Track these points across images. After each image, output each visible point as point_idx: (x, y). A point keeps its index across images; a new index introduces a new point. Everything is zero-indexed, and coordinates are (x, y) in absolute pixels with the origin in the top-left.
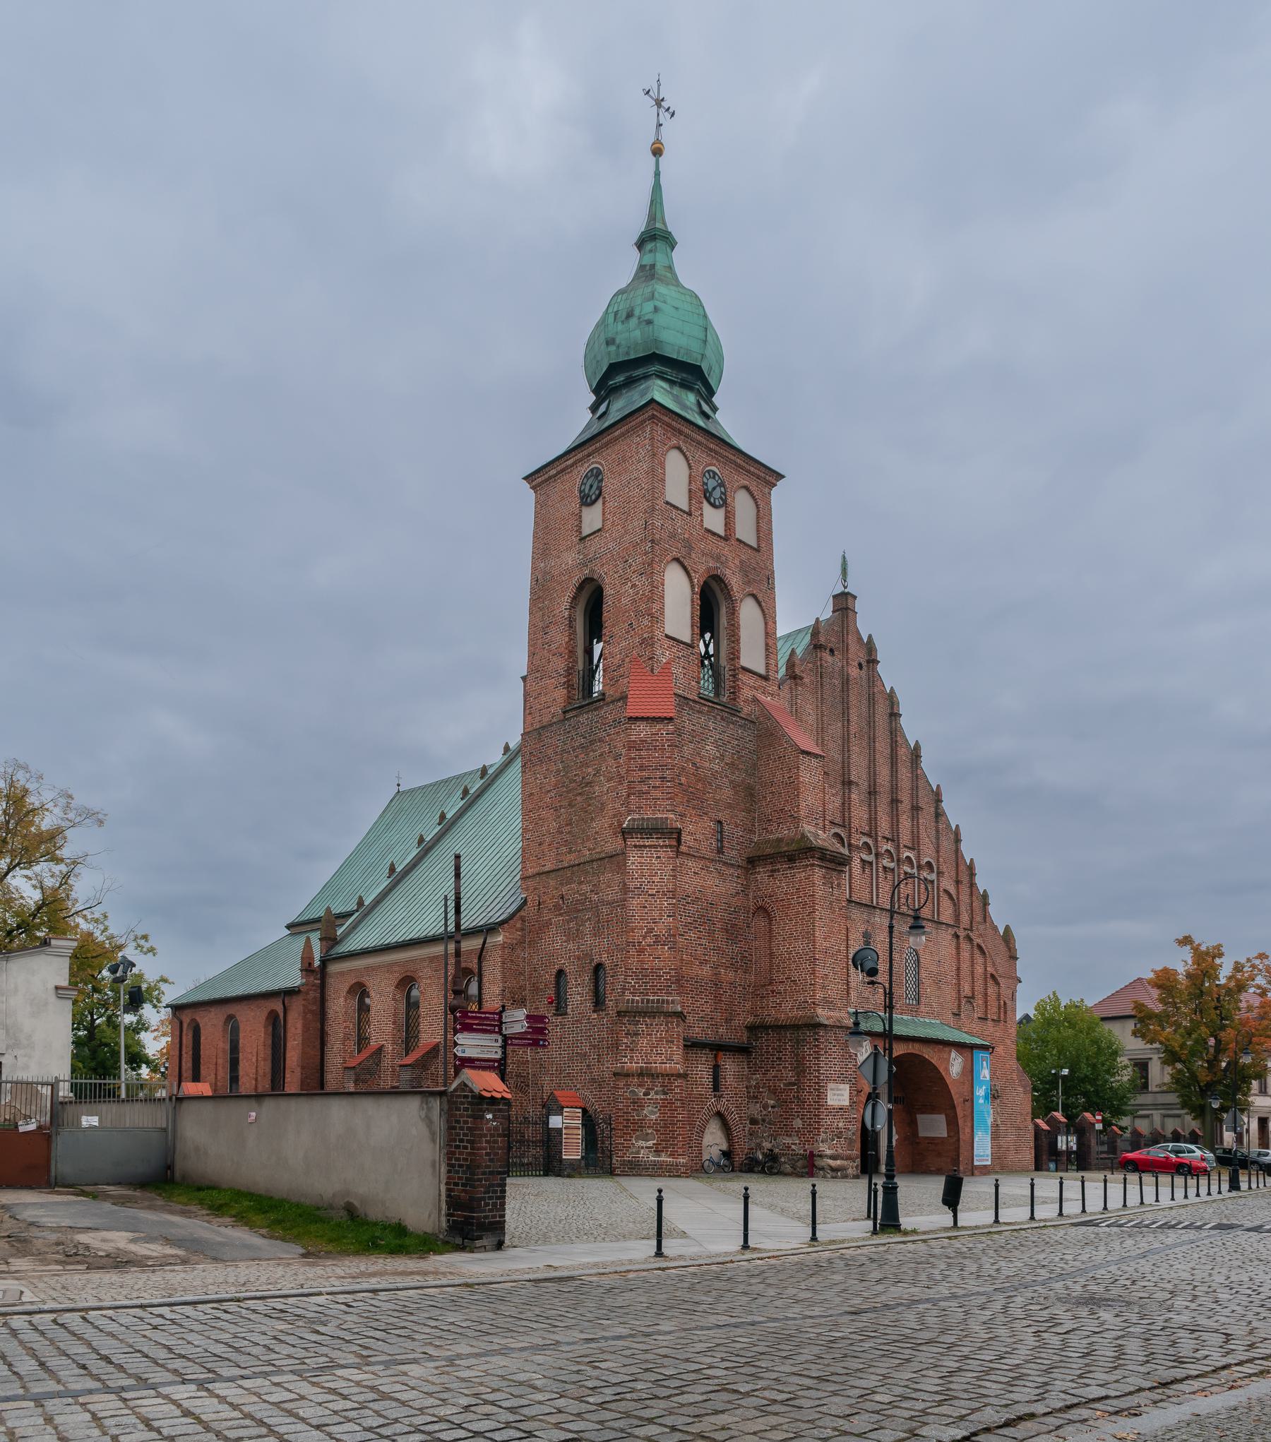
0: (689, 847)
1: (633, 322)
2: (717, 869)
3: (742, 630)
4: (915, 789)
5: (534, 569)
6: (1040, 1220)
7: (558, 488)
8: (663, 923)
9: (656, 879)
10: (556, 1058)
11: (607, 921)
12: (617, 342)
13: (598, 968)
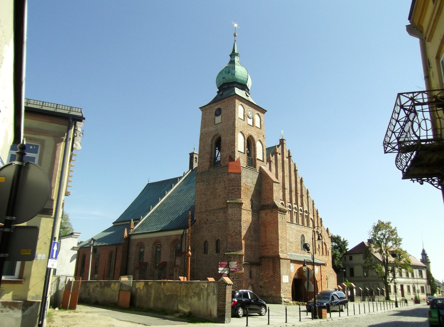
1: (230, 74)
3: (257, 149)
4: (302, 190)
5: (201, 130)
6: (342, 317)
12: (226, 78)
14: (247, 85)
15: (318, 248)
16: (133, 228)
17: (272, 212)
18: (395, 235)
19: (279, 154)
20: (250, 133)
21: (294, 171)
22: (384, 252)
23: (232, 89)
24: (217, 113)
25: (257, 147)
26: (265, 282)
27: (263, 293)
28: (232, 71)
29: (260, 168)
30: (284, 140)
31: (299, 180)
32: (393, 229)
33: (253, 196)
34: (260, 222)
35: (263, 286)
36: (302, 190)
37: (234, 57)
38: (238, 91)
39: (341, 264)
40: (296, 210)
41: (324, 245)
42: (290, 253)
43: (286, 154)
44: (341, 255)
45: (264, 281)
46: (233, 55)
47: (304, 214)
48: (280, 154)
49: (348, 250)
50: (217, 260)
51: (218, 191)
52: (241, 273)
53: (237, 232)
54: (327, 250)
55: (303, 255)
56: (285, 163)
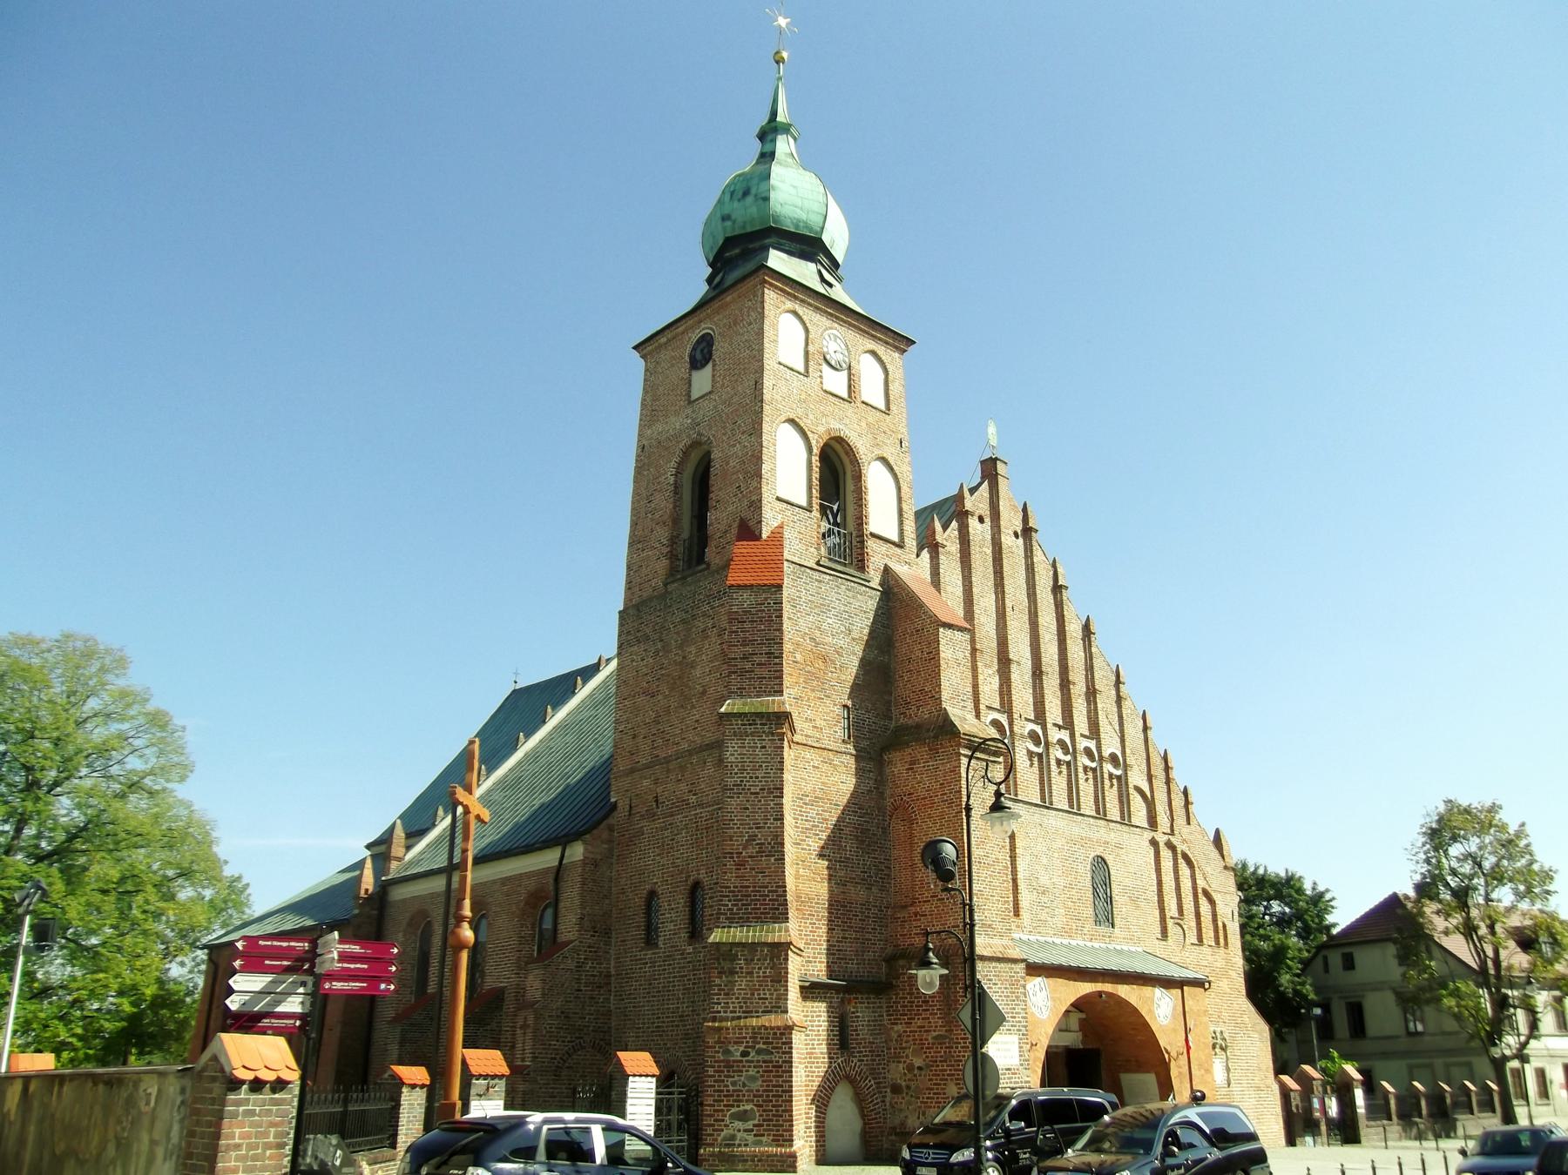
0: (806, 736)
1: (750, 199)
2: (842, 762)
4: (1090, 668)
7: (665, 355)
8: (769, 828)
9: (760, 774)
10: (643, 1006)
11: (706, 828)
12: (733, 217)
13: (696, 886)
14: (824, 238)
15: (1177, 916)
16: (400, 854)
17: (934, 751)
18: (1523, 857)
19: (976, 518)
20: (835, 425)
21: (1049, 589)
22: (1483, 931)
23: (758, 258)
24: (699, 356)
25: (868, 487)
26: (910, 1068)
27: (906, 1117)
28: (758, 189)
29: (887, 570)
30: (998, 462)
31: (1074, 629)
32: (1512, 832)
33: (856, 690)
34: (889, 802)
35: (904, 1084)
36: (1090, 668)
37: (774, 141)
38: (778, 260)
39: (1308, 987)
40: (1066, 752)
41: (1203, 901)
42: (1039, 938)
43: (1011, 521)
44: (1308, 951)
45: (908, 1061)
46: (770, 131)
47: (1105, 770)
48: (981, 520)
49: (1335, 931)
50: (692, 973)
51: (697, 672)
52: (779, 1028)
53: (764, 844)
54: (1220, 924)
55: (1102, 945)
56: (1004, 556)
